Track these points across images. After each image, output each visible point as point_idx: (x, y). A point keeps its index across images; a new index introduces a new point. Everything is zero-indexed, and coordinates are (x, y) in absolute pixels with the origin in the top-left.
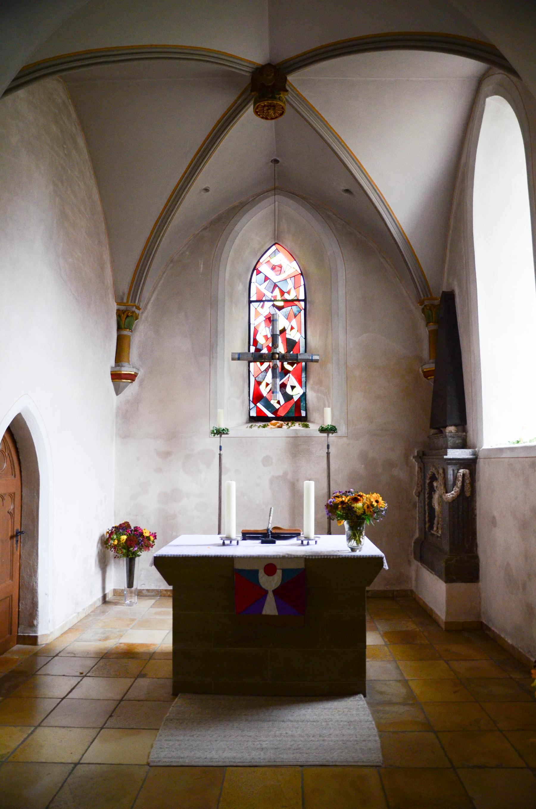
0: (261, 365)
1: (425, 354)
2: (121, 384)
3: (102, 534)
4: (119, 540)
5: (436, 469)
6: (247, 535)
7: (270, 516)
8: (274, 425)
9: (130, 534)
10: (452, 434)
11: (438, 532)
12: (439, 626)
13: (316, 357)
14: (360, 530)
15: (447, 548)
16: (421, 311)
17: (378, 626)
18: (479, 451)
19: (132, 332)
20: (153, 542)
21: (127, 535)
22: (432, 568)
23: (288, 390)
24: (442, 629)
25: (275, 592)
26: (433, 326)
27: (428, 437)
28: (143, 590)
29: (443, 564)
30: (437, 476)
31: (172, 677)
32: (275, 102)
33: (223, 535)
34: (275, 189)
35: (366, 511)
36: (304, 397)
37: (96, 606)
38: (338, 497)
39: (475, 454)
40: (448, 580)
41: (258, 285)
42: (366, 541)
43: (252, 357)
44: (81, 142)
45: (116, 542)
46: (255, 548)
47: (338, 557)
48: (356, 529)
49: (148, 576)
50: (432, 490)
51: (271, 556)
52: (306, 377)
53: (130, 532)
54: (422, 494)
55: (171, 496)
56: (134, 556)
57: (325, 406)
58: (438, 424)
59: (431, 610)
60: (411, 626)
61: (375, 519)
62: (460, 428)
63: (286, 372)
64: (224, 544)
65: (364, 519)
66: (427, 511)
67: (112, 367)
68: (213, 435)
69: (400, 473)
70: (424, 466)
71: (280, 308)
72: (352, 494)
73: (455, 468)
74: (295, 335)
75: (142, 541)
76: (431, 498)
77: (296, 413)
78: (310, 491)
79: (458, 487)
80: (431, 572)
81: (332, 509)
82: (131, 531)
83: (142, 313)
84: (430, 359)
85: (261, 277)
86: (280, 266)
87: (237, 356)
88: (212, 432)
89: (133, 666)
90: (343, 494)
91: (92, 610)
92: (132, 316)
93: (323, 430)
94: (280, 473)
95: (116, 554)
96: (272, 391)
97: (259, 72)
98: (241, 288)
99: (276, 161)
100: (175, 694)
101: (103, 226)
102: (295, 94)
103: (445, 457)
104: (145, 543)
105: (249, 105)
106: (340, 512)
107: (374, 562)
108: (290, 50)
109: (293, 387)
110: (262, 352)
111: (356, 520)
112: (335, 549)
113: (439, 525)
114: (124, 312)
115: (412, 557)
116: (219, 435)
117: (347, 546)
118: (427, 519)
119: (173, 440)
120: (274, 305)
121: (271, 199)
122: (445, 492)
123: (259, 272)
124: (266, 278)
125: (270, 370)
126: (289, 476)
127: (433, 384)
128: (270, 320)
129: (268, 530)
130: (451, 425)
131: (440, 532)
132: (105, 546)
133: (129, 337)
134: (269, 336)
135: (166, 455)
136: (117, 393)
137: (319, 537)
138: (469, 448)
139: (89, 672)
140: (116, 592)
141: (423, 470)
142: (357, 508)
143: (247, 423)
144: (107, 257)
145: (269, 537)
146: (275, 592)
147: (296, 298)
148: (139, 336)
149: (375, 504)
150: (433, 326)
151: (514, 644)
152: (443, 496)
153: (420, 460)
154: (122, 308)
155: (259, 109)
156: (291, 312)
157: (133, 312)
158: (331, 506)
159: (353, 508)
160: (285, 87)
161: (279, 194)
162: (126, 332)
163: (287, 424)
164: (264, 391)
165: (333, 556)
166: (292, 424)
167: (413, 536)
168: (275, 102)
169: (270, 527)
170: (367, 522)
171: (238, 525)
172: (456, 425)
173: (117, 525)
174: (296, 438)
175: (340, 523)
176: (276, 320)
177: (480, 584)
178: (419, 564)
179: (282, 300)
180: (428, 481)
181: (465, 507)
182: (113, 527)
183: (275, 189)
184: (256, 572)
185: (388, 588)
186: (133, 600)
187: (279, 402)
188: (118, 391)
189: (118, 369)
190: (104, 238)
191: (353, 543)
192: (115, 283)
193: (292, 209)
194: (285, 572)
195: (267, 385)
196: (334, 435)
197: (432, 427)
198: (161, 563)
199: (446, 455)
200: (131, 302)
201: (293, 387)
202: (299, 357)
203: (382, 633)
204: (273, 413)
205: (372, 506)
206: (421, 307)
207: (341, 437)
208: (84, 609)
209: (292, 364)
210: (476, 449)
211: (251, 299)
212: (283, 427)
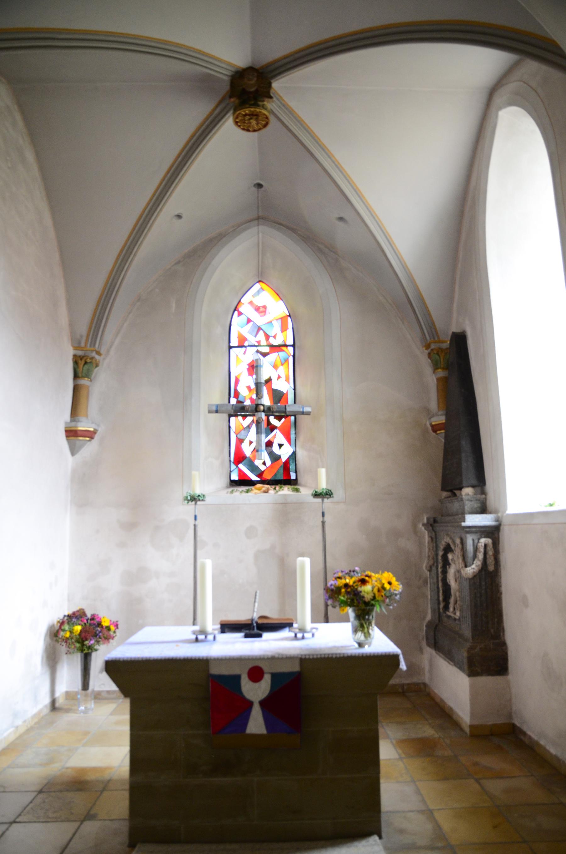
0: (244, 419)
2: (78, 442)
3: (51, 624)
4: (71, 632)
5: (451, 538)
6: (227, 627)
7: (255, 602)
8: (259, 489)
9: (85, 624)
10: (469, 497)
11: (455, 614)
12: (461, 729)
14: (368, 619)
15: (467, 632)
16: (427, 356)
17: (389, 732)
18: (502, 516)
19: (91, 381)
20: (115, 632)
21: (82, 625)
22: (449, 656)
23: (275, 449)
24: (466, 733)
26: (441, 373)
27: (440, 501)
28: (102, 691)
29: (465, 654)
30: (452, 547)
31: (127, 818)
32: (258, 110)
33: (197, 628)
34: (258, 218)
35: (377, 596)
36: (294, 457)
37: (42, 715)
38: (340, 578)
40: (472, 673)
41: (239, 326)
42: (377, 633)
43: (233, 409)
44: (30, 156)
46: (236, 646)
47: (342, 655)
48: (364, 619)
49: (102, 682)
50: (446, 563)
51: (256, 656)
52: (295, 433)
53: (85, 621)
54: (434, 568)
55: (136, 576)
56: (90, 651)
57: (318, 467)
58: (451, 484)
59: (451, 709)
60: (428, 731)
61: (388, 605)
62: (478, 489)
63: (272, 428)
64: (197, 640)
65: (373, 606)
66: (441, 589)
67: (66, 423)
68: (186, 502)
69: (408, 544)
70: (436, 535)
71: (264, 355)
72: (357, 573)
73: (475, 536)
74: (283, 385)
75: (100, 632)
76: (445, 572)
77: (285, 476)
78: (305, 567)
79: (479, 560)
80: (449, 663)
81: (333, 593)
82: (87, 620)
83: (104, 359)
84: (439, 411)
85: (243, 319)
86: (265, 307)
87: (214, 408)
88: (186, 499)
89: (80, 801)
90: (346, 574)
91: (36, 720)
92: (91, 362)
95: (69, 649)
97: (239, 76)
98: (219, 331)
99: (259, 186)
101: (57, 256)
102: (281, 103)
103: (463, 524)
104: (103, 634)
105: (227, 116)
106: (348, 598)
107: (388, 662)
108: (275, 50)
109: (280, 446)
110: (245, 404)
111: (363, 607)
112: (338, 644)
113: (458, 606)
114: (81, 358)
115: (424, 643)
116: (193, 503)
117: (352, 640)
118: (441, 598)
120: (258, 352)
121: (254, 230)
122: (463, 565)
123: (240, 314)
124: (249, 321)
125: (254, 426)
127: (443, 440)
128: (253, 368)
129: (252, 620)
130: (468, 487)
131: (458, 614)
132: (55, 638)
133: (88, 387)
134: (253, 386)
135: (130, 526)
137: (316, 629)
138: (490, 513)
139: (20, 815)
140: (68, 695)
141: (434, 539)
142: (365, 592)
143: (227, 487)
144: (61, 292)
145: (253, 629)
147: (283, 343)
148: (100, 385)
149: (387, 586)
150: (441, 373)
151: (559, 754)
152: (462, 572)
153: (431, 528)
154: (80, 353)
155: (240, 118)
156: (278, 359)
157: (92, 358)
158: (332, 590)
159: (361, 592)
160: (269, 92)
161: (263, 225)
162: (84, 382)
163: (275, 489)
164: (247, 450)
165: (336, 654)
166: (281, 488)
167: (424, 618)
168: (258, 110)
169: (256, 616)
170: (377, 609)
171: (215, 611)
172: (473, 487)
173: (70, 612)
175: (343, 610)
176: (261, 366)
177: (510, 677)
178: (433, 652)
179: (267, 345)
180: (441, 553)
182: (65, 616)
183: (258, 218)
184: (237, 678)
186: (88, 706)
187: (264, 463)
188: (73, 451)
189: (73, 424)
190: (58, 270)
191: (360, 636)
192: (72, 325)
193: (278, 240)
194: (275, 677)
195: (251, 443)
196: (330, 500)
197: (443, 489)
198: (114, 668)
199: (464, 521)
200: (90, 346)
201: (280, 446)
202: (288, 409)
203: (394, 742)
204: (258, 476)
205: (383, 588)
206: (427, 352)
207: (338, 502)
208: (25, 721)
209: (279, 418)
210: (500, 515)
211: (232, 345)
212: (270, 492)
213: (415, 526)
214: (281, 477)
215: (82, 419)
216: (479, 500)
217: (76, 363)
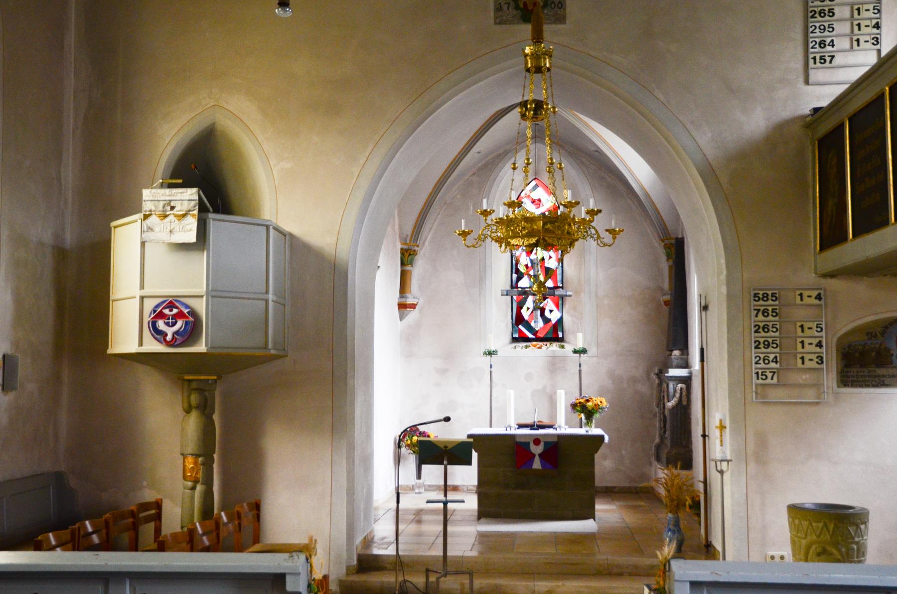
1: (666, 286)
6: (521, 426)
13: (569, 293)
23: (547, 313)
25: (540, 455)
39: (691, 373)
45: (409, 442)
69: (644, 388)
77: (554, 334)
86: (539, 200)
93: (575, 352)
100: (479, 518)
109: (551, 311)
114: (406, 250)
119: (449, 358)
126: (548, 390)
133: (410, 272)
135: (443, 372)
136: (401, 320)
146: (540, 455)
148: (418, 271)
154: (405, 247)
162: (408, 268)
164: (525, 313)
174: (553, 357)
181: (683, 410)
184: (528, 444)
185: (632, 485)
189: (403, 300)
194: (546, 443)
195: (528, 309)
201: (551, 311)
213: (648, 375)
214: (550, 335)
215: (408, 295)
217: (402, 254)
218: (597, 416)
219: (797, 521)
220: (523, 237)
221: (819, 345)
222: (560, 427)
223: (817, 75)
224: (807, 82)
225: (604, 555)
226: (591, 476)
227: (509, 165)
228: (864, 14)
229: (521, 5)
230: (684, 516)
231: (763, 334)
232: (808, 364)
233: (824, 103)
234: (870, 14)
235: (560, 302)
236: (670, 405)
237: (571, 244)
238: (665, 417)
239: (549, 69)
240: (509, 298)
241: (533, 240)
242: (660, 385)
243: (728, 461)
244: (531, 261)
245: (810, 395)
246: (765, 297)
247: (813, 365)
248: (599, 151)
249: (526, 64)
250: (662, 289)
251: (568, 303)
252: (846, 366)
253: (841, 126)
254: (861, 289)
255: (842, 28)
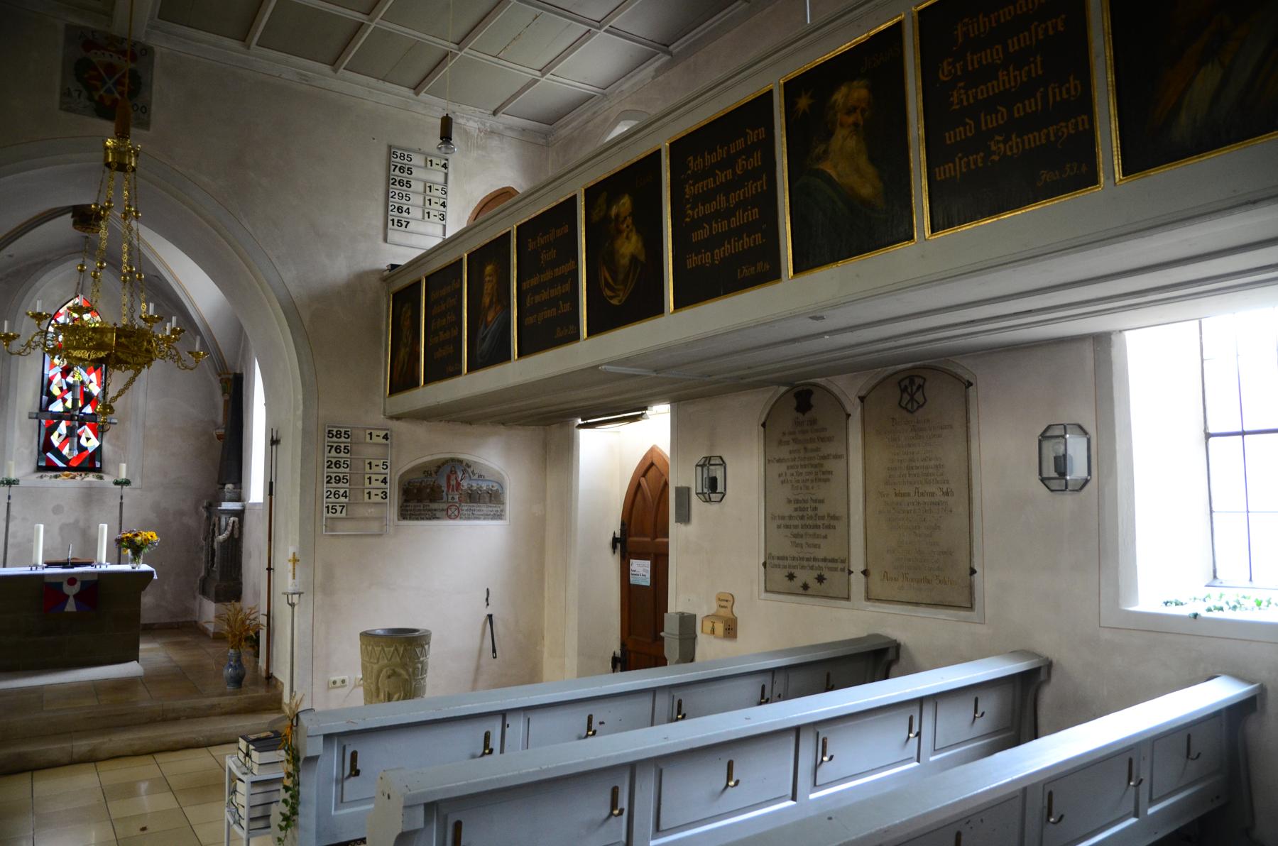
1: (220, 419)
22: (209, 598)
25: (75, 596)
39: (244, 506)
40: (217, 601)
69: (191, 521)
77: (90, 463)
78: (104, 533)
93: (117, 483)
94: (71, 521)
96: (63, 444)
109: (88, 439)
146: (75, 596)
164: (55, 440)
181: (234, 546)
184: (61, 584)
194: (83, 583)
201: (88, 439)
213: (197, 509)
214: (86, 465)
216: (473, 497)
218: (146, 550)
219: (370, 648)
220: (89, 349)
221: (384, 481)
222: (100, 564)
223: (394, 235)
224: (385, 240)
225: (145, 701)
226: (138, 615)
227: (80, 261)
228: (434, 193)
229: (96, 98)
230: (246, 651)
231: (335, 469)
232: (374, 499)
233: (402, 262)
234: (439, 193)
235: (99, 432)
236: (221, 538)
237: (149, 362)
238: (213, 550)
239: (134, 169)
240: (36, 421)
241: (103, 354)
242: (209, 518)
243: (300, 594)
244: (68, 384)
245: (374, 527)
246: (339, 434)
247: (378, 499)
248: (159, 277)
249: (106, 157)
250: (215, 423)
251: (107, 436)
252: (406, 501)
253: (419, 282)
254: (420, 431)
255: (417, 200)
